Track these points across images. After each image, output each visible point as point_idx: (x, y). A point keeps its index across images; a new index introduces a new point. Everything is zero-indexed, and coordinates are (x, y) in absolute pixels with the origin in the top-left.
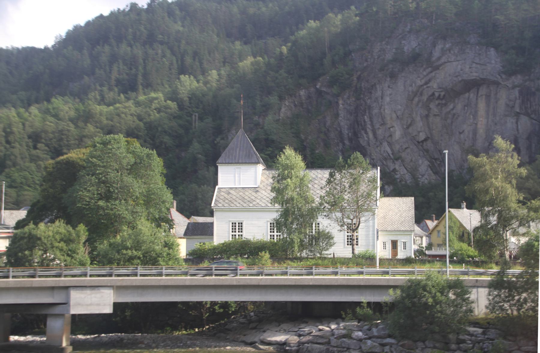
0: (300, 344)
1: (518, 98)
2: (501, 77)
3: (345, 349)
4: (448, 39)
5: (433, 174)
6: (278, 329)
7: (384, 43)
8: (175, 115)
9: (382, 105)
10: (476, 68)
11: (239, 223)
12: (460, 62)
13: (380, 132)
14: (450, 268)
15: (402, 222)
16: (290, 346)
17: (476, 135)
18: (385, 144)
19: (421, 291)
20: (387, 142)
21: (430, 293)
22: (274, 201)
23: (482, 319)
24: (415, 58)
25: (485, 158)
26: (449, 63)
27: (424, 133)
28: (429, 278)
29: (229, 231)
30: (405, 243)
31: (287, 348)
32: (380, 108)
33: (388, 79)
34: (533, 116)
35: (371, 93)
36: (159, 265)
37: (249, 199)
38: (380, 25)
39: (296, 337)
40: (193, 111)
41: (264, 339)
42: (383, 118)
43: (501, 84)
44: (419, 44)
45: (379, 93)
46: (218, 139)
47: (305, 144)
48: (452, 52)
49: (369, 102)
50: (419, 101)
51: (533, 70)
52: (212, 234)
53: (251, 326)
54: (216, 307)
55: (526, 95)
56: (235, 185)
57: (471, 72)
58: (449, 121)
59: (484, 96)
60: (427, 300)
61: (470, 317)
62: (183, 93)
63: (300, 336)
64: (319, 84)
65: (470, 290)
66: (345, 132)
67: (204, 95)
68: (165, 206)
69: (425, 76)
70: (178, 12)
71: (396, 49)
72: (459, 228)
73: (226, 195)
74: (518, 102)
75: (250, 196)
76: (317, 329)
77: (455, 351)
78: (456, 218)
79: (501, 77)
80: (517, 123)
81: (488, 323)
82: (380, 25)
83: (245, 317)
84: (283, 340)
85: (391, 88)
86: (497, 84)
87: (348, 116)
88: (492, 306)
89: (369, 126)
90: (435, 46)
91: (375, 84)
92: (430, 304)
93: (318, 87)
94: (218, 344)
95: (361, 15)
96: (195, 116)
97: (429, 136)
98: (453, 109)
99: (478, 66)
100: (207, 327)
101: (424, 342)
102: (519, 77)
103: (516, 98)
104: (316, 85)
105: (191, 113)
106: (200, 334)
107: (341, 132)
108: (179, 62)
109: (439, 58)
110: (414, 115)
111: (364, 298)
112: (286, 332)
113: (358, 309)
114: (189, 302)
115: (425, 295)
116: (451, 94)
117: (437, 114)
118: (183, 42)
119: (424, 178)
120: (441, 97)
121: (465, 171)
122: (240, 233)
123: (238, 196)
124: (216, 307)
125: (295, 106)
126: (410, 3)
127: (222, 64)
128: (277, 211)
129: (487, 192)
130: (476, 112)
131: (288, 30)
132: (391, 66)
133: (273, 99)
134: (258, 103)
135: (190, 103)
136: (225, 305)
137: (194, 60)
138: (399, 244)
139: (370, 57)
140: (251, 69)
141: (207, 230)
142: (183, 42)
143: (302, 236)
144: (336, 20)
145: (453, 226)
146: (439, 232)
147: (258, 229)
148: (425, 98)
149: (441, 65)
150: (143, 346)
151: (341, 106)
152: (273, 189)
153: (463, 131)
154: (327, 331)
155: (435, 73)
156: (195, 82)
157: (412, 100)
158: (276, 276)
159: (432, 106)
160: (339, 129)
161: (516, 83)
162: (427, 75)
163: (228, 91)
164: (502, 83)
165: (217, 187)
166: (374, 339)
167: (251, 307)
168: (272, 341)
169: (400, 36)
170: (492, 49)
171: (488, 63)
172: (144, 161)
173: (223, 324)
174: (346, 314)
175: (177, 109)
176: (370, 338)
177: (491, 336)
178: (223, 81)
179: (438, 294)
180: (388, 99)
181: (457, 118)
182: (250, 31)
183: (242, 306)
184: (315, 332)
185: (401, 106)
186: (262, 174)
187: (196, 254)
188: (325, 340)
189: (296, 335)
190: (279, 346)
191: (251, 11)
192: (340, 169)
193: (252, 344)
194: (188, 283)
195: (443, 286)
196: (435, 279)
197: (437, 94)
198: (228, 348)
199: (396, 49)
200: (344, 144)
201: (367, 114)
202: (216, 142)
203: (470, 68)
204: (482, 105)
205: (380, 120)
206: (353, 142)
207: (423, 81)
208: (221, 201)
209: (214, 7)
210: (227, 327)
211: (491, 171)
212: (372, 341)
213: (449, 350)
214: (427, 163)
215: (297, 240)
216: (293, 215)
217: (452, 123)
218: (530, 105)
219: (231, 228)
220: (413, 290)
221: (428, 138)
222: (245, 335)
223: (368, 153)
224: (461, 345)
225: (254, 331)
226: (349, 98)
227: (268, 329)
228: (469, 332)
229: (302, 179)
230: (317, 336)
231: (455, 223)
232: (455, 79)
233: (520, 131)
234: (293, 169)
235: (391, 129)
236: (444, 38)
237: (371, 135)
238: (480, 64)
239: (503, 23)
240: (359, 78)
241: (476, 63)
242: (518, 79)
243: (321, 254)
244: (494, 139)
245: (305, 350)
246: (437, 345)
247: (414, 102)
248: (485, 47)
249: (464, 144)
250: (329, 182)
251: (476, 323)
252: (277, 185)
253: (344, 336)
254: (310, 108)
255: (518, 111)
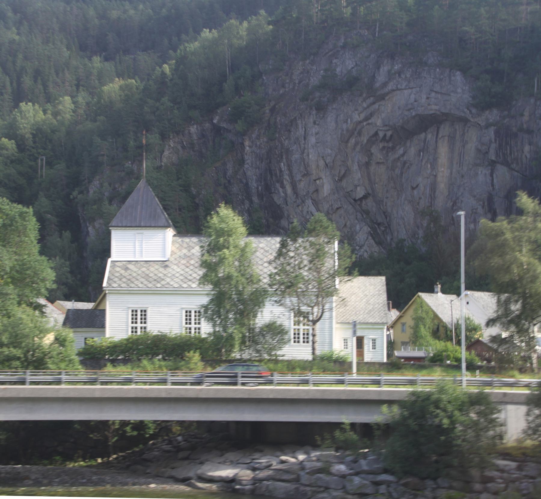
0: (256, 481)
1: (493, 141)
2: (470, 111)
3: (322, 489)
4: (397, 58)
5: (375, 245)
6: (222, 459)
7: (308, 61)
8: (13, 158)
9: (305, 148)
10: (435, 99)
11: (141, 311)
12: (414, 90)
13: (301, 185)
14: (466, 377)
15: (370, 311)
16: (240, 484)
17: (435, 192)
18: (309, 202)
19: (432, 409)
20: (312, 199)
21: (445, 410)
22: (204, 280)
23: (513, 448)
24: (350, 85)
25: (505, 223)
26: (398, 92)
27: (363, 188)
28: (442, 390)
29: (127, 322)
30: (374, 340)
31: (238, 487)
32: (303, 153)
33: (314, 112)
34: (514, 166)
35: (289, 131)
36: (48, 368)
37: (155, 278)
38: (303, 37)
39: (249, 472)
40: (39, 153)
41: (202, 474)
42: (307, 166)
43: (470, 121)
44: (356, 65)
45: (301, 131)
46: (75, 193)
47: (197, 201)
48: (403, 76)
49: (286, 143)
50: (356, 144)
51: (514, 103)
52: (102, 326)
53: (181, 455)
54: (128, 429)
55: (505, 136)
56: (135, 257)
57: (429, 105)
58: (397, 171)
59: (446, 138)
60: (441, 420)
61: (499, 447)
62: (25, 128)
63: (254, 469)
64: (217, 117)
65: (500, 407)
66: (253, 184)
67: (53, 132)
68: (45, 285)
69: (365, 109)
70: (10, 14)
71: (326, 70)
72: (433, 320)
73: (123, 272)
74: (493, 146)
75: (156, 272)
76: (278, 460)
77: (480, 492)
78: (428, 306)
79: (470, 111)
80: (492, 175)
81: (524, 454)
82: (303, 37)
83: (170, 442)
84: (231, 475)
85: (318, 125)
86: (464, 121)
87: (258, 163)
88: (533, 430)
89: (286, 177)
90: (379, 68)
91: (295, 118)
92: (445, 426)
93: (215, 121)
94: (136, 481)
95: (273, 23)
96: (42, 160)
97: (370, 192)
98: (403, 155)
99: (439, 96)
100: (115, 456)
101: (435, 479)
102: (495, 111)
103: (491, 141)
104: (212, 120)
105: (36, 155)
106: (106, 465)
107: (247, 184)
108: (15, 84)
109: (385, 84)
110: (349, 163)
111: (346, 417)
112: (234, 464)
113: (337, 433)
114: (89, 421)
115: (438, 414)
116: (403, 133)
117: (381, 161)
118: (20, 56)
119: (362, 250)
120: (387, 138)
121: (419, 241)
122: (143, 325)
123: (140, 272)
124: (128, 429)
125: (183, 147)
126: (344, 7)
127: (74, 88)
128: (207, 294)
129: (508, 270)
130: (435, 159)
131: (166, 41)
132: (317, 94)
133: (154, 138)
134: (131, 142)
135: (34, 142)
136: (140, 426)
137: (35, 81)
138: (365, 341)
139: (288, 81)
140: (120, 96)
141: (96, 320)
142: (20, 56)
143: (244, 330)
144: (241, 30)
145: (426, 316)
146: (403, 324)
147: (167, 319)
148: (364, 139)
149: (387, 94)
150: (31, 482)
151: (247, 148)
152: (204, 264)
153: (417, 186)
154: (294, 464)
155: (379, 106)
156: (41, 112)
157: (347, 142)
158: (150, 385)
159: (374, 150)
160: (244, 181)
161: (491, 120)
162: (368, 107)
163: (89, 125)
164: (472, 120)
165: (109, 260)
166: (363, 476)
167: (176, 429)
168: (214, 477)
169: (330, 53)
170: (458, 73)
171: (452, 91)
172: (17, 222)
173: (137, 452)
174: (323, 439)
175: (16, 150)
176: (357, 474)
177: (532, 473)
178: (81, 111)
179: (457, 413)
180: (313, 140)
181: (409, 168)
182: (103, 42)
183: (164, 427)
184: (275, 465)
185: (331, 150)
186: (173, 242)
187: (89, 354)
188: (293, 475)
189: (248, 469)
190: (225, 484)
191: (114, 14)
192: (294, 235)
193: (185, 481)
194: (97, 395)
195: (463, 402)
196: (451, 391)
197: (381, 134)
198: (153, 486)
199: (326, 70)
200: (251, 202)
201: (285, 160)
202: (71, 197)
203: (428, 98)
204: (443, 151)
205: (302, 169)
206: (265, 199)
207: (363, 116)
208: (116, 279)
209: (61, 8)
210: (145, 456)
211: (514, 241)
212: (362, 478)
213: (471, 491)
214: (366, 229)
215: (237, 336)
216: (231, 299)
217: (402, 173)
218: (511, 151)
219: (130, 317)
220: (419, 408)
221: (369, 194)
222: (173, 468)
223: (286, 215)
224: (489, 485)
225: (186, 462)
226: (258, 137)
227: (207, 460)
228: (497, 466)
229: (243, 250)
230: (280, 470)
231: (427, 313)
232: (406, 113)
233: (497, 187)
234: (229, 236)
235: (318, 182)
236: (392, 57)
237: (289, 190)
238: (441, 93)
239: (473, 37)
240: (272, 110)
241: (436, 92)
242: (493, 115)
243: (270, 355)
244: (516, 196)
245: (264, 489)
246: (455, 484)
247: (349, 145)
248: (448, 71)
249: (418, 203)
250: (280, 254)
251: (506, 455)
252: (206, 257)
253: (320, 471)
254: (204, 151)
255: (493, 158)
